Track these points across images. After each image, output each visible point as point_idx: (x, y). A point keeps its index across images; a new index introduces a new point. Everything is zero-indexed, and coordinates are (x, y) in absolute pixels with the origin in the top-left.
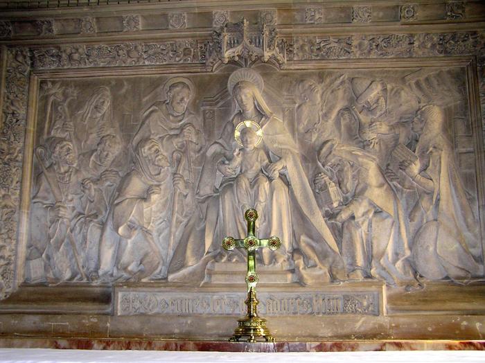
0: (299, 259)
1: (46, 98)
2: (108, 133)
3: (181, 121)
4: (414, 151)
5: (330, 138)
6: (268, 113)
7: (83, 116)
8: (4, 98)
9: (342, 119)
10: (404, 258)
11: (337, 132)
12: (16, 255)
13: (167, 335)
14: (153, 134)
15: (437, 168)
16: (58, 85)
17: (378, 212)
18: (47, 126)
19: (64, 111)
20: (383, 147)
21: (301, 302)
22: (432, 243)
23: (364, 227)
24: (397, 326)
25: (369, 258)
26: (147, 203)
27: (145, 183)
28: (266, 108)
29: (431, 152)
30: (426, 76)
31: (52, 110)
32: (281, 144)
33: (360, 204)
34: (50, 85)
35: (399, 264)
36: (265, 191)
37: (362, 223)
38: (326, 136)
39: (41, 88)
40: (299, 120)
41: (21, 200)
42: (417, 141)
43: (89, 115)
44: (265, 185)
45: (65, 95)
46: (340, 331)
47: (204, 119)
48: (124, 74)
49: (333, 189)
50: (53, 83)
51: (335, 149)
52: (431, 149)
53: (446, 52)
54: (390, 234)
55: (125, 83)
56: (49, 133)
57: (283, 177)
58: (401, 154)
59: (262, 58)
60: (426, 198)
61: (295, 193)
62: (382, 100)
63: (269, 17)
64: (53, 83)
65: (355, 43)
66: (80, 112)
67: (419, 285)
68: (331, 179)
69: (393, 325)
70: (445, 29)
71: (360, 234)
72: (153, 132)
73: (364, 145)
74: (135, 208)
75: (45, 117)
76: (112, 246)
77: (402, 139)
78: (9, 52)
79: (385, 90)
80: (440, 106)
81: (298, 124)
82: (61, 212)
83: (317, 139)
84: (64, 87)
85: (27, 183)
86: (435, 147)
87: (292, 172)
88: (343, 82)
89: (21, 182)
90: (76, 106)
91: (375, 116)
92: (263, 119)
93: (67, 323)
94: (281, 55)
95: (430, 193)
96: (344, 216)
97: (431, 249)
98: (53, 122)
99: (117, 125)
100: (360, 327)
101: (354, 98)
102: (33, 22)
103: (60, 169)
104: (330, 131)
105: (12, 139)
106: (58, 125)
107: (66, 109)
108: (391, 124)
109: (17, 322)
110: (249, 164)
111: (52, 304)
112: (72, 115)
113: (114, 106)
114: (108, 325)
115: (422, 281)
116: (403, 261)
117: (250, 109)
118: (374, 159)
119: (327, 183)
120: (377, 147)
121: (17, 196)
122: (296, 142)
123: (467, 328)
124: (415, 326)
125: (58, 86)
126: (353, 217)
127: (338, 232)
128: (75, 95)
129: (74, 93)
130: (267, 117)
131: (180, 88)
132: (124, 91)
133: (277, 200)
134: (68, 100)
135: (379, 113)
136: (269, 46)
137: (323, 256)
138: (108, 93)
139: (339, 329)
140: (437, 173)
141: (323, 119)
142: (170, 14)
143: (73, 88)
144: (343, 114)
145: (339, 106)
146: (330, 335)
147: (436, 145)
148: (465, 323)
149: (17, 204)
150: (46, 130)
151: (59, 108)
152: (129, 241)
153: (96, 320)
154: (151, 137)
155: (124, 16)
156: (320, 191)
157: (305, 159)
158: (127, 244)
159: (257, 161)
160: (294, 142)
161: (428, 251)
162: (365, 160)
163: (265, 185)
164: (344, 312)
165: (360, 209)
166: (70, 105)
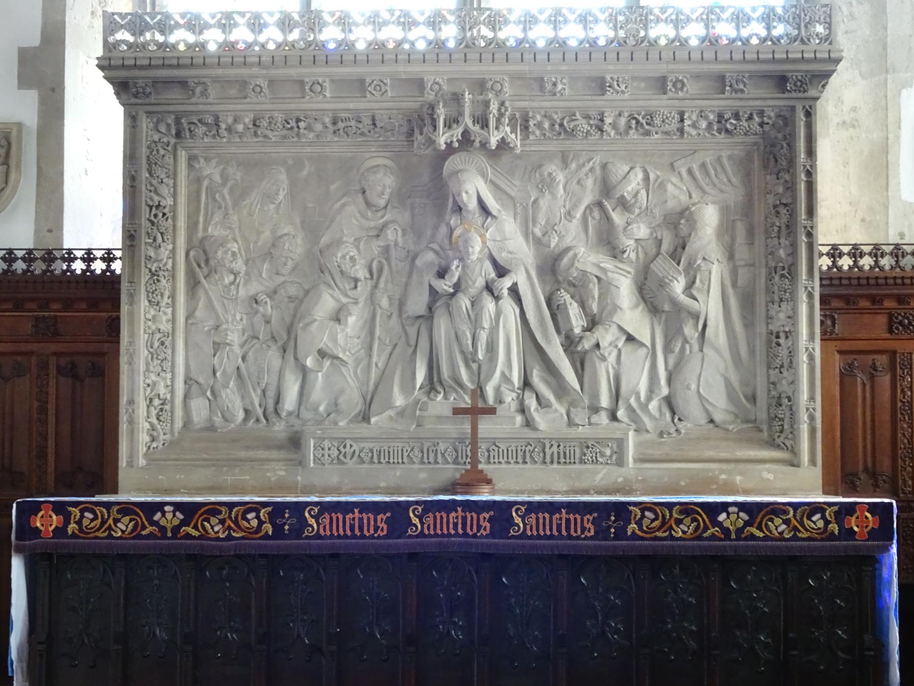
0: (531, 398)
1: (198, 181)
2: (286, 231)
3: (382, 217)
4: (678, 264)
5: (574, 243)
6: (494, 212)
7: (250, 208)
8: (146, 185)
9: (590, 218)
10: (659, 397)
11: (583, 236)
12: (172, 392)
13: (371, 489)
14: (346, 236)
15: (706, 287)
16: (214, 162)
17: (630, 338)
18: (201, 219)
19: (224, 199)
20: (641, 255)
21: (531, 450)
22: (695, 379)
23: (612, 359)
24: (643, 480)
25: (616, 396)
26: (342, 327)
27: (337, 300)
28: (492, 203)
29: (699, 266)
30: (701, 161)
31: (207, 198)
32: (511, 253)
33: (607, 330)
34: (202, 161)
35: (653, 406)
36: (490, 315)
37: (610, 354)
38: (568, 242)
39: (190, 166)
40: (535, 222)
41: (173, 320)
42: (684, 248)
43: (259, 206)
44: (489, 305)
45: (225, 179)
46: (578, 485)
47: (413, 216)
48: (304, 151)
49: (574, 310)
50: (207, 159)
51: (578, 261)
52: (699, 262)
53: (727, 131)
54: (643, 369)
55: (306, 163)
56: (205, 229)
57: (514, 291)
58: (662, 266)
59: (487, 145)
60: (691, 322)
61: (527, 316)
62: (643, 193)
63: (498, 87)
64: (207, 159)
65: (608, 120)
66: (244, 203)
67: (676, 430)
68: (572, 297)
69: (640, 478)
70: (725, 107)
71: (604, 373)
72: (346, 232)
73: (616, 253)
74: (327, 332)
75: (198, 207)
76: (296, 381)
77: (665, 247)
78: (149, 120)
79: (647, 178)
80: (714, 203)
81: (534, 225)
82: (229, 338)
83: (557, 244)
84: (221, 167)
85: (181, 298)
86: (704, 259)
87: (524, 290)
88: (592, 170)
89: (173, 296)
90: (241, 194)
91: (633, 214)
92: (489, 219)
93: (248, 478)
94: (513, 136)
95: (696, 316)
96: (587, 344)
97: (693, 387)
98: (210, 213)
99: (298, 221)
100: (602, 479)
101: (606, 188)
102: (183, 84)
103: (224, 279)
104: (574, 233)
105: (159, 239)
106: (217, 217)
107: (227, 197)
108: (653, 225)
109: (178, 477)
110: (470, 279)
111: (139, 408)
112: (236, 205)
113: (292, 196)
114: (299, 478)
115: (681, 426)
116: (659, 400)
117: (473, 205)
118: (629, 273)
119: (568, 303)
120: (633, 256)
121: (170, 316)
122: (530, 249)
123: (726, 483)
124: (666, 479)
125: (214, 165)
126: (598, 346)
127: (580, 364)
128: (238, 178)
129: (236, 174)
130: (494, 217)
131: (381, 174)
132: (305, 173)
133: (504, 326)
134: (229, 184)
135: (637, 211)
136: (497, 128)
137: (561, 389)
138: (283, 177)
139: (576, 483)
140: (706, 293)
141: (565, 217)
142: (368, 80)
143: (235, 168)
144: (591, 211)
145: (588, 199)
146: (565, 489)
147: (706, 257)
148: (723, 476)
149: (169, 326)
150: (201, 226)
151: (217, 196)
152: (320, 374)
153: (283, 473)
154: (344, 239)
155: (306, 80)
156: (556, 311)
157: (541, 271)
158: (317, 377)
159: (481, 274)
160: (527, 250)
161: (690, 389)
162: (617, 276)
163: (489, 305)
164: (582, 462)
165: (607, 336)
166: (232, 191)
